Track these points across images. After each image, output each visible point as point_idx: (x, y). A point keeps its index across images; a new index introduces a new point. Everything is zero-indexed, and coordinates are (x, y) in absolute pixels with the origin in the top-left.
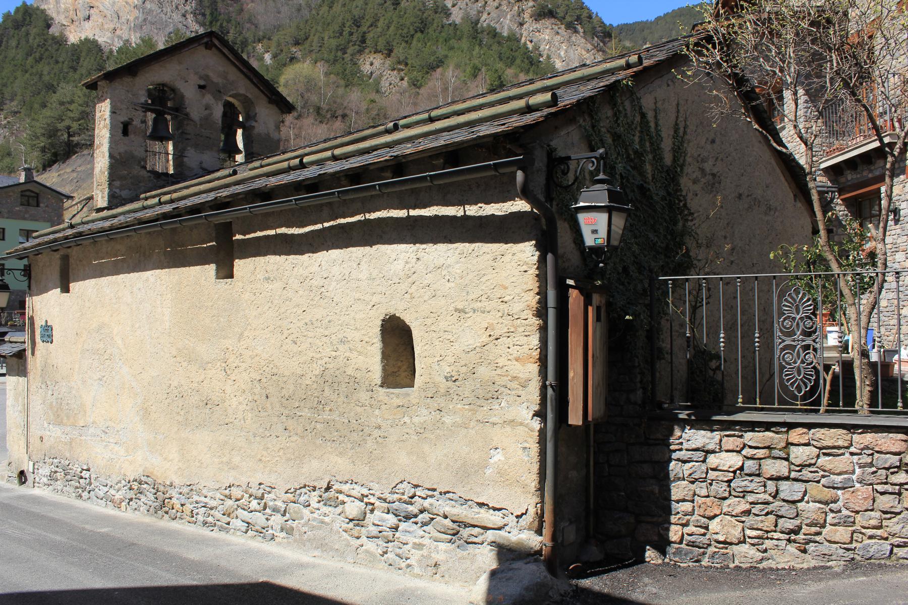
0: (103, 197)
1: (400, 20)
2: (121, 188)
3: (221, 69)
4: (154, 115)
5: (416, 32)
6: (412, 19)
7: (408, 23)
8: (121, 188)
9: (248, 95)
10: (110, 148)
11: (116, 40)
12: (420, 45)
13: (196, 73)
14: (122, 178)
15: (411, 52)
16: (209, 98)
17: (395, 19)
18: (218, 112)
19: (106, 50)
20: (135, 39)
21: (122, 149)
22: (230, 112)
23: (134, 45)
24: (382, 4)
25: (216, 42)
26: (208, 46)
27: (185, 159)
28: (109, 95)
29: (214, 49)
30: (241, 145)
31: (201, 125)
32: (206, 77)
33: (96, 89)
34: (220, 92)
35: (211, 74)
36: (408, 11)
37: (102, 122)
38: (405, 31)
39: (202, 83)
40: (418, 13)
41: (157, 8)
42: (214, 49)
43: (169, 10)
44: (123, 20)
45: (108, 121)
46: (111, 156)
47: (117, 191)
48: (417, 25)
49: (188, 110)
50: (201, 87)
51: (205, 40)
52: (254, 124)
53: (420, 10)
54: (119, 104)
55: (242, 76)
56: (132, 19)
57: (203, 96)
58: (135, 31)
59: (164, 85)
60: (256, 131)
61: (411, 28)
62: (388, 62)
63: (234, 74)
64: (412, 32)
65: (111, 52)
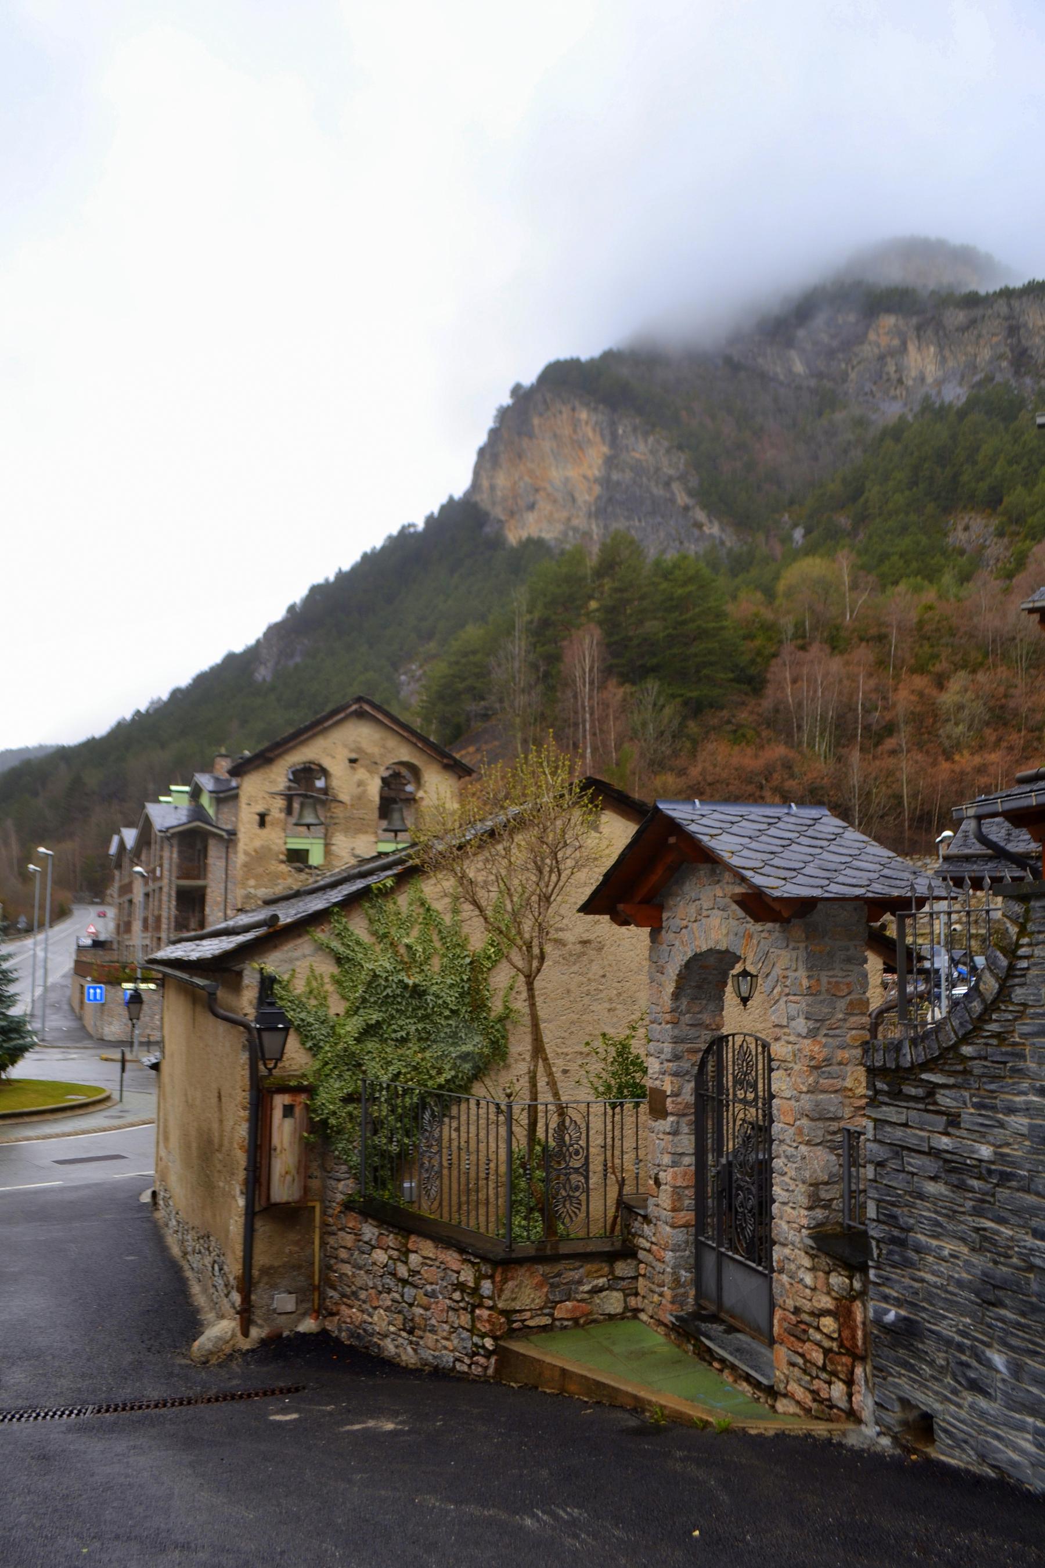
11: (571, 533)
23: (932, 349)
25: (367, 708)
32: (359, 750)
34: (376, 763)
39: (354, 756)
50: (353, 761)
62: (995, 522)
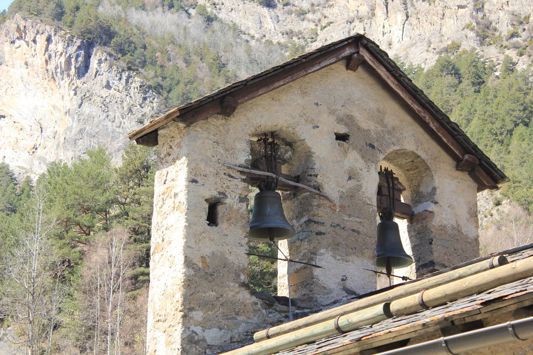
0: (169, 343)
1: (488, 108)
2: (205, 325)
3: (372, 105)
4: (257, 191)
5: (517, 125)
6: (508, 105)
7: (502, 111)
8: (205, 325)
9: (420, 153)
10: (187, 246)
11: (36, 163)
12: (524, 145)
13: (332, 112)
14: (206, 305)
15: (511, 157)
16: (353, 159)
17: (479, 107)
18: (370, 184)
19: (21, 179)
20: (67, 157)
21: (207, 249)
22: (388, 184)
24: (456, 86)
25: (367, 57)
26: (351, 63)
27: (317, 272)
28: (185, 150)
29: (360, 69)
30: (408, 248)
31: (342, 207)
33: (155, 142)
34: (373, 147)
35: (357, 115)
36: (500, 94)
37: (169, 202)
38: (498, 124)
39: (343, 130)
40: (518, 94)
41: (100, 112)
42: (360, 69)
43: (118, 114)
44: (48, 132)
45: (183, 198)
46: (188, 263)
47: (198, 329)
48: (517, 113)
49: (319, 179)
50: (341, 138)
51: (348, 52)
52: (432, 207)
53: (520, 90)
54: (202, 166)
55: (408, 119)
56: (61, 130)
57: (346, 152)
58: (66, 149)
59: (273, 134)
60: (436, 222)
61: (508, 119)
63: (394, 115)
64: (510, 126)
65: (28, 181)
